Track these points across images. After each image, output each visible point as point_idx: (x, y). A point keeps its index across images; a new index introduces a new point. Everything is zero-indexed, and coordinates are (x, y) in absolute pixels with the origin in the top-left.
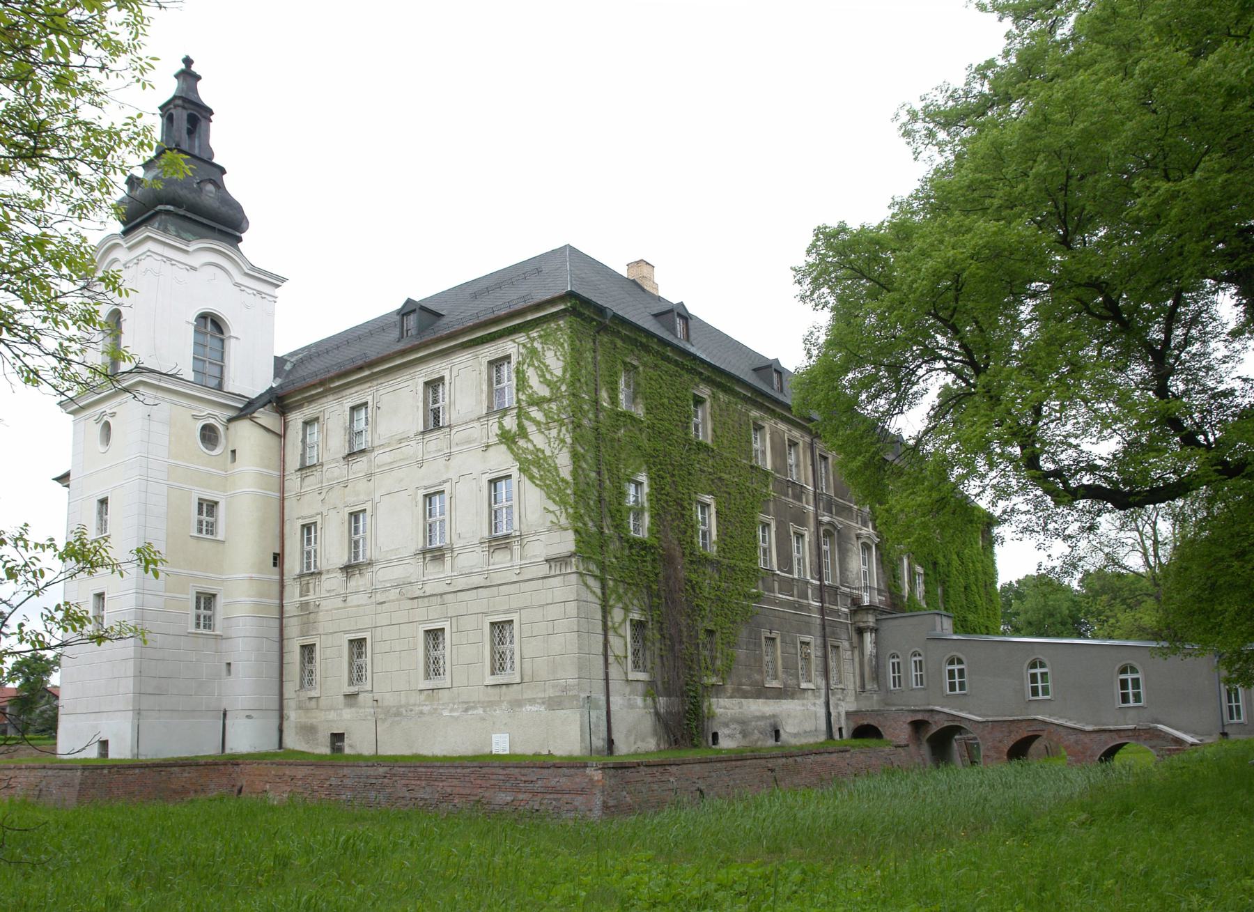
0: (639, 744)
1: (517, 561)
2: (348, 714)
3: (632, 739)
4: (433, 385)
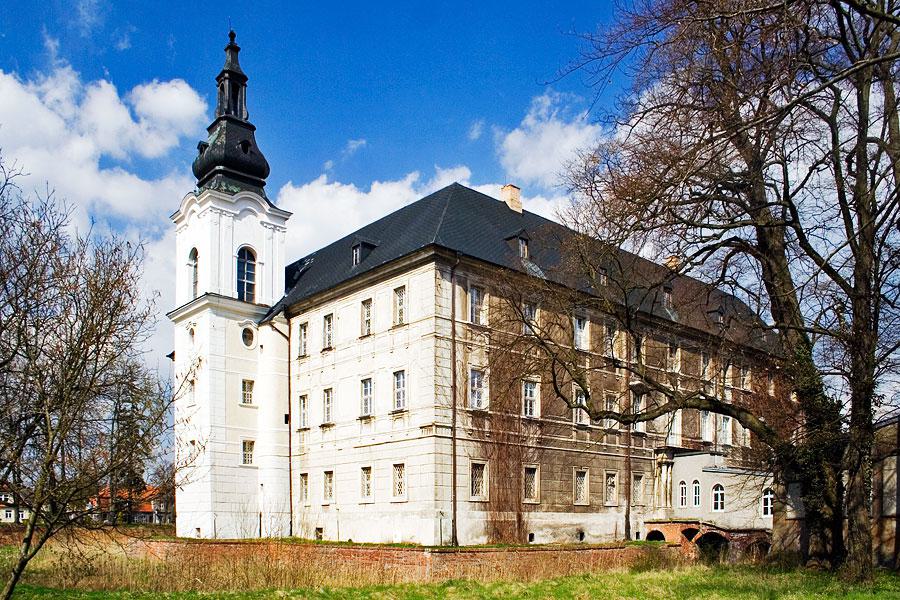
0: (475, 540)
1: (407, 427)
2: (324, 516)
3: (470, 536)
4: (367, 303)
